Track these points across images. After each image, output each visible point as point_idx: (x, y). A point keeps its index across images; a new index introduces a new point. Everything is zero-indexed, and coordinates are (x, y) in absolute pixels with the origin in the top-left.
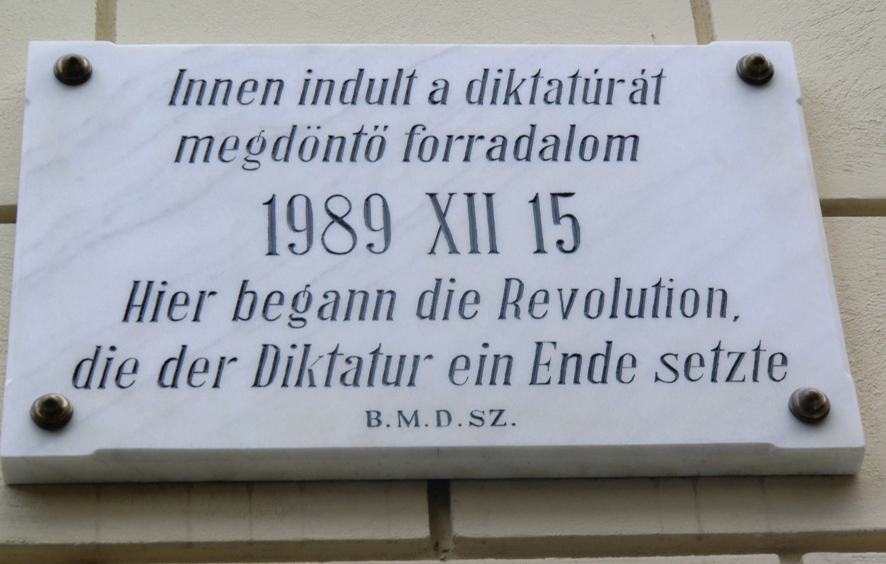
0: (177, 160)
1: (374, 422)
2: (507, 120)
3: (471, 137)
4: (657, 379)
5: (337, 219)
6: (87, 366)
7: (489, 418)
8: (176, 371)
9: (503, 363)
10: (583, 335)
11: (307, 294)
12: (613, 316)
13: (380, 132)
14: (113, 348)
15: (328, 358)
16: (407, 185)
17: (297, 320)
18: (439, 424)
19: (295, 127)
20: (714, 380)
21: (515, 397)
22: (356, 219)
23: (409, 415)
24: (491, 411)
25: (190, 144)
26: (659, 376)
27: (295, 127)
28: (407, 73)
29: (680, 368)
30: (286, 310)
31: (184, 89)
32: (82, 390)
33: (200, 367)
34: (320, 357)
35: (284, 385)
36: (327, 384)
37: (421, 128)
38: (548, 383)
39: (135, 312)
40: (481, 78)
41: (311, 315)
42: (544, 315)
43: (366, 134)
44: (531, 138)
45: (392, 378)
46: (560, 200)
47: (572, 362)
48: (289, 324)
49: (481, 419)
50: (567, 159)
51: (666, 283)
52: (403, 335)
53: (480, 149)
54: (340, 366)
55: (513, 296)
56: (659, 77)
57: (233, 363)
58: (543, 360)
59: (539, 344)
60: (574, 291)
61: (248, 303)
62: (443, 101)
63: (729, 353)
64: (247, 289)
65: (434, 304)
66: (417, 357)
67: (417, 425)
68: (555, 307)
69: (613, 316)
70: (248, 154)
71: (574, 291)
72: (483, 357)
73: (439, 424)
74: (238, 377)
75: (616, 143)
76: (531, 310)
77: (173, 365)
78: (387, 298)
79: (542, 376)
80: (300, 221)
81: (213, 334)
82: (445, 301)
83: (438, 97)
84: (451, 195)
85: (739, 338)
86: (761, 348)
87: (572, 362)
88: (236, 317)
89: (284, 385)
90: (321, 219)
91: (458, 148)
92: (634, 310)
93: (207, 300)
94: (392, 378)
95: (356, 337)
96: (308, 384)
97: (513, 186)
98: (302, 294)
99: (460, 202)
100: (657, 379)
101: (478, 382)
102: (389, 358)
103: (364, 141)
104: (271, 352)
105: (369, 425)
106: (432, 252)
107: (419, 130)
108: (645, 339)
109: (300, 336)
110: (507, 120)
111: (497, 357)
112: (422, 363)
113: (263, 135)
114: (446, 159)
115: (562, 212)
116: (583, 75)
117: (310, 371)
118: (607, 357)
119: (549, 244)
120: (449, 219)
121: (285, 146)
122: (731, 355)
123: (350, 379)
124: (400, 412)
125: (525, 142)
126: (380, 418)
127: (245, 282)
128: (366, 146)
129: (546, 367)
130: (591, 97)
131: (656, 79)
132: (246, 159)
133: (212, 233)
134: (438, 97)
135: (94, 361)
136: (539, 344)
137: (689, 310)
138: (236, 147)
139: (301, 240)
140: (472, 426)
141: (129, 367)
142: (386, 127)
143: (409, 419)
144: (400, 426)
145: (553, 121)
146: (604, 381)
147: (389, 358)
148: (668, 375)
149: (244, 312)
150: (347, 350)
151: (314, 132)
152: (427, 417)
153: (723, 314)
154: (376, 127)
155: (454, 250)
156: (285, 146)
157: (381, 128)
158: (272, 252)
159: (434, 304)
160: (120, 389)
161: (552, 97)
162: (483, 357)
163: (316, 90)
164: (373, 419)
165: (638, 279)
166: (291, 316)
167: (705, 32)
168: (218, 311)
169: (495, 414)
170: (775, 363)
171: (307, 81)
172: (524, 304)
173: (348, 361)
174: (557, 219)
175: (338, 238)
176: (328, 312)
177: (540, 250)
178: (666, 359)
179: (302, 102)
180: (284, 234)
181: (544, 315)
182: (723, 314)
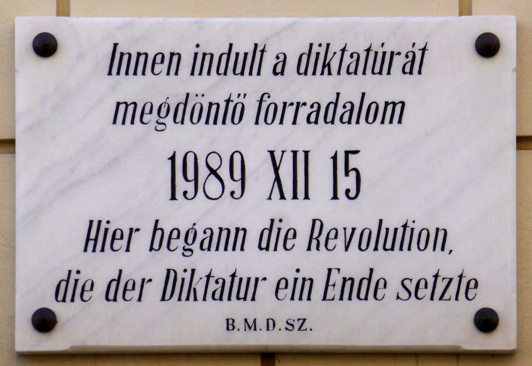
0: (114, 122)
1: (231, 327)
2: (317, 89)
3: (298, 104)
4: (398, 298)
5: (213, 172)
6: (63, 284)
7: (297, 325)
8: (118, 289)
9: (308, 283)
10: (354, 263)
11: (194, 230)
12: (376, 249)
13: (241, 99)
14: (78, 272)
15: (205, 279)
16: (254, 141)
17: (187, 251)
18: (268, 329)
19: (188, 95)
20: (432, 299)
21: (312, 309)
22: (224, 173)
23: (251, 322)
24: (299, 320)
25: (122, 107)
26: (400, 296)
27: (188, 95)
28: (260, 48)
29: (413, 290)
30: (181, 243)
31: (120, 62)
32: (61, 303)
33: (130, 287)
34: (201, 278)
35: (180, 299)
36: (204, 299)
37: (267, 95)
38: (333, 299)
39: (91, 244)
40: (307, 52)
41: (196, 247)
42: (334, 248)
43: (232, 101)
44: (336, 104)
45: (242, 295)
46: (351, 156)
47: (348, 283)
48: (183, 254)
49: (292, 325)
50: (358, 122)
51: (410, 225)
52: (250, 262)
53: (304, 112)
54: (212, 286)
55: (316, 235)
56: (424, 50)
57: (149, 283)
58: (331, 283)
59: (330, 270)
60: (354, 229)
61: (161, 238)
62: (282, 73)
63: (444, 279)
64: (158, 227)
65: (274, 237)
66: (257, 279)
67: (255, 329)
68: (340, 242)
69: (376, 249)
70: (159, 118)
71: (354, 229)
72: (296, 279)
73: (268, 329)
74: (153, 291)
75: (390, 107)
76: (326, 245)
77: (114, 284)
78: (241, 233)
79: (329, 296)
80: (191, 175)
81: (140, 262)
82: (183, 292)
83: (279, 69)
84: (283, 152)
85: (449, 266)
86: (463, 275)
87: (348, 283)
88: (151, 249)
89: (180, 299)
90: (203, 172)
91: (290, 111)
92: (388, 246)
93: (135, 235)
94: (242, 295)
95: (220, 263)
96: (193, 299)
97: (324, 142)
98: (191, 230)
99: (288, 158)
100: (398, 298)
101: (292, 299)
102: (241, 279)
103: (231, 105)
104: (172, 274)
105: (228, 329)
106: (270, 198)
107: (266, 97)
108: (395, 266)
109: (188, 263)
110: (317, 89)
111: (304, 279)
112: (260, 282)
113: (168, 101)
114: (281, 122)
115: (351, 167)
116: (374, 49)
117: (195, 289)
118: (369, 280)
119: (341, 193)
120: (280, 172)
121: (182, 111)
122: (445, 280)
123: (217, 296)
124: (246, 320)
125: (332, 107)
126: (234, 324)
127: (157, 221)
128: (228, 112)
129: (333, 287)
130: (377, 70)
131: (421, 51)
132: (157, 122)
133: (133, 186)
134: (279, 69)
135: (68, 281)
136: (330, 270)
137: (422, 246)
138: (151, 112)
139: (190, 187)
140: (287, 331)
141: (88, 287)
142: (245, 95)
143: (250, 324)
144: (245, 330)
145: (350, 88)
146: (366, 299)
147: (241, 279)
148: (404, 294)
149: (156, 246)
150: (216, 274)
151: (199, 99)
152: (261, 324)
153: (443, 249)
154: (239, 95)
155: (282, 197)
156: (182, 111)
157: (242, 96)
158: (173, 198)
159: (274, 237)
160: (83, 302)
161: (352, 70)
162: (296, 279)
163: (203, 63)
164: (230, 325)
165: (393, 222)
166: (184, 247)
167: (465, 9)
168: (141, 241)
169: (301, 321)
170: (468, 286)
171: (196, 54)
172: (322, 239)
173: (217, 282)
174: (347, 174)
175: (213, 187)
176: (206, 246)
177: (335, 197)
178: (405, 282)
179: (192, 74)
180: (181, 185)
181: (334, 248)
182: (443, 249)
